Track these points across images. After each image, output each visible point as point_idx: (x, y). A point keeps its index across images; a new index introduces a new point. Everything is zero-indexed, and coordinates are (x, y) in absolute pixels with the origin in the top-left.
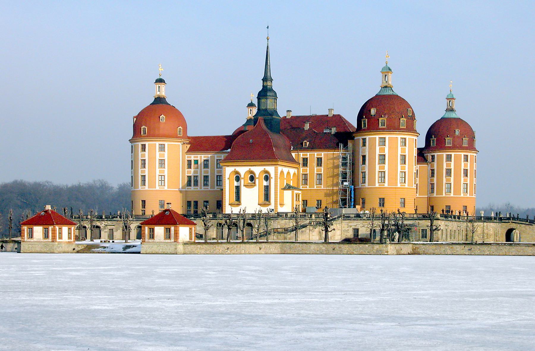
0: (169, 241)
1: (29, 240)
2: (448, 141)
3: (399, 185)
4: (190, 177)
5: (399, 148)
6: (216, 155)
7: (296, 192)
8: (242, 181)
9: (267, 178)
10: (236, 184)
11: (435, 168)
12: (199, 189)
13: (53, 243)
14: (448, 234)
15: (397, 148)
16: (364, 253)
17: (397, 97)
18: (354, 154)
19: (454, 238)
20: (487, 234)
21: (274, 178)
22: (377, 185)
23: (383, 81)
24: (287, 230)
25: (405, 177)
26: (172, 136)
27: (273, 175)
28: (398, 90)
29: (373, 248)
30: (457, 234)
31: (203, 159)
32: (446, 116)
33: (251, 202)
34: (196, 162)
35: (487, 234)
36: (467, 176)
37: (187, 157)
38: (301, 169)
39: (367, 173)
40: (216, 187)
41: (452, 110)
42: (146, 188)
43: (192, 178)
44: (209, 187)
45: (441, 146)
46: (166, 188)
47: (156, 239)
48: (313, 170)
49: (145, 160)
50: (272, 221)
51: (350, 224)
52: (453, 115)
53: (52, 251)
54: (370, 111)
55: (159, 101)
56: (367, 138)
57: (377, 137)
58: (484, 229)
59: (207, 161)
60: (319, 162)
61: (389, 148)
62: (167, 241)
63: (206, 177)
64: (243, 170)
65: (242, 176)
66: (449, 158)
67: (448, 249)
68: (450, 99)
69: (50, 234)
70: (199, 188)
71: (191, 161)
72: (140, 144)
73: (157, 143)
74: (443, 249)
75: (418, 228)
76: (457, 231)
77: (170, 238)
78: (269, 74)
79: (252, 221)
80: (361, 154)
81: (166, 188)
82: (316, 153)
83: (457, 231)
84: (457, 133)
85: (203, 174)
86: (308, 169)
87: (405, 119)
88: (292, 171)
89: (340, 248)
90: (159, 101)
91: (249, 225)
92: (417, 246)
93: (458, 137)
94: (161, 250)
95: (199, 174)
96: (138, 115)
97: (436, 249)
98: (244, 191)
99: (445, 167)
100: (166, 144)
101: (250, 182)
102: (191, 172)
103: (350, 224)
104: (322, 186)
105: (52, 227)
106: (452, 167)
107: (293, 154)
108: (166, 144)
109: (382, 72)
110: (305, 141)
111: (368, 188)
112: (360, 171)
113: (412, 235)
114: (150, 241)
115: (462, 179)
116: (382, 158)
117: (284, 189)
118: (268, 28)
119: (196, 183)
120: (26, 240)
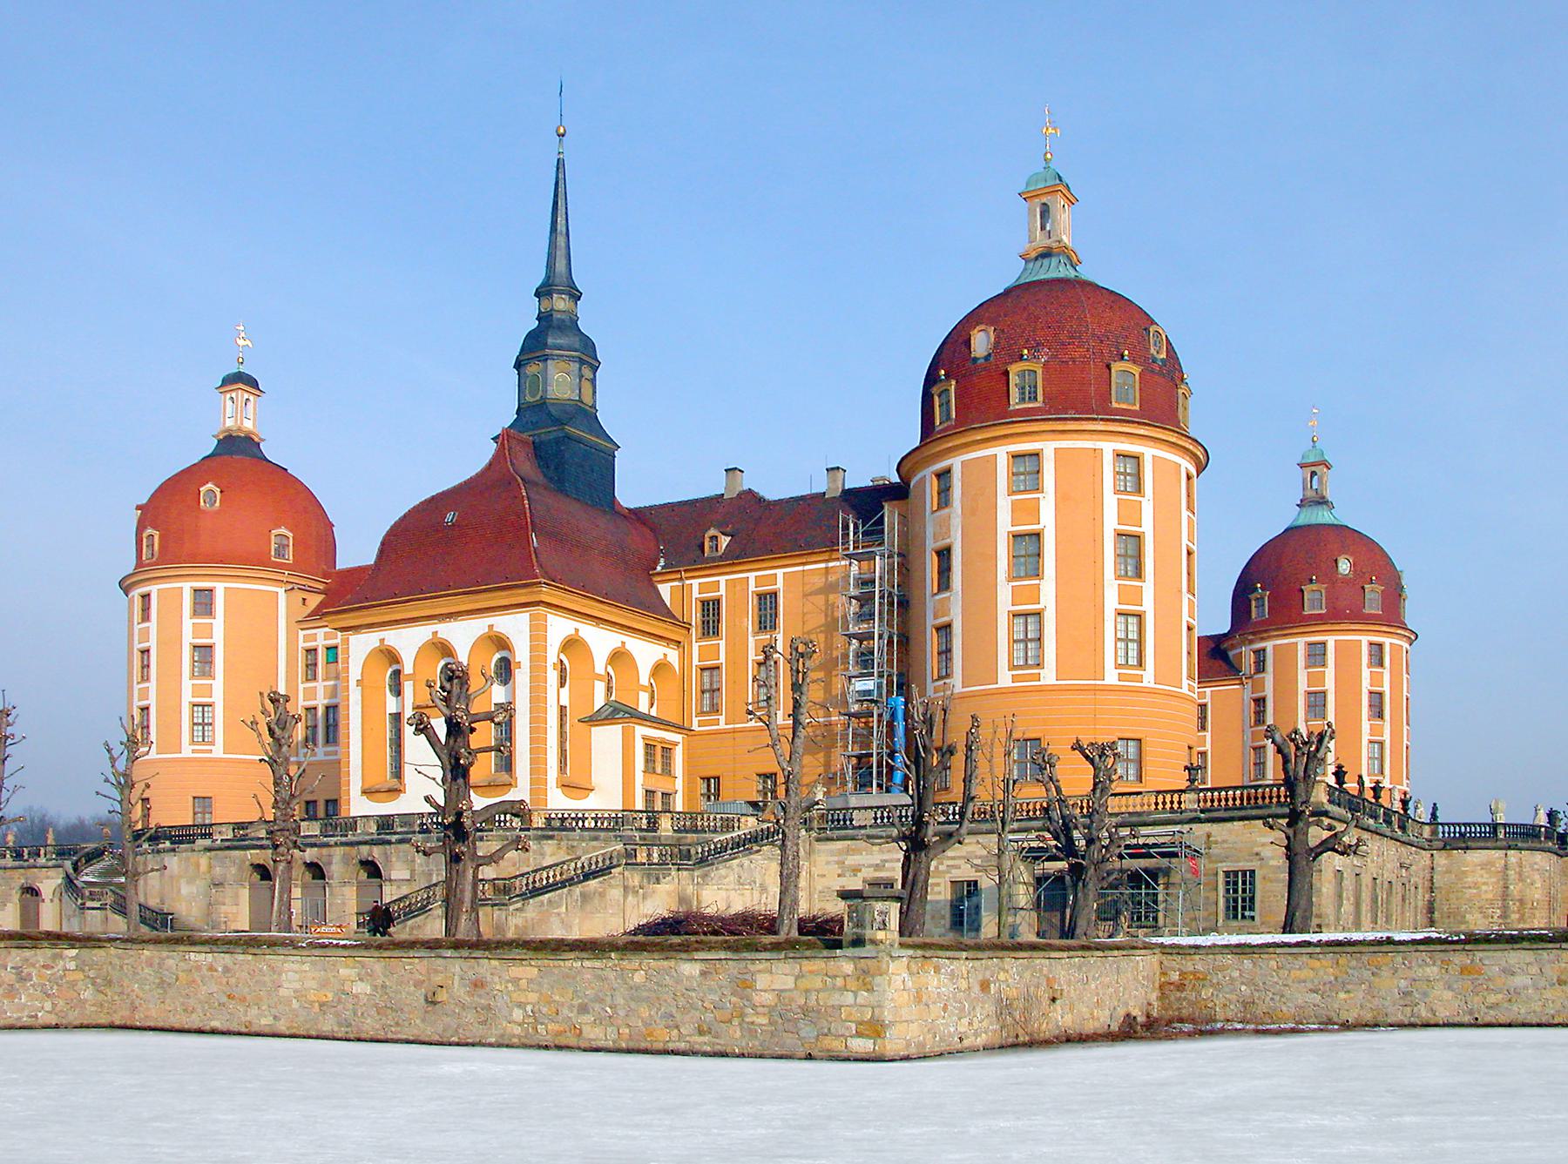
2: (1314, 598)
3: (1111, 677)
5: (1110, 502)
7: (641, 731)
11: (1269, 692)
14: (1366, 896)
16: (663, 1037)
18: (906, 564)
19: (1388, 920)
20: (1521, 901)
21: (526, 664)
22: (1005, 679)
23: (1031, 231)
24: (506, 890)
25: (1140, 642)
26: (256, 560)
27: (522, 654)
29: (744, 986)
30: (1396, 900)
32: (1301, 522)
35: (1521, 901)
36: (1380, 716)
38: (695, 647)
41: (1322, 501)
43: (320, 711)
45: (1288, 615)
46: (218, 751)
48: (741, 644)
51: (851, 860)
52: (1322, 516)
55: (237, 448)
58: (1505, 878)
61: (1061, 499)
65: (408, 669)
66: (1317, 654)
67: (1440, 986)
68: (1314, 467)
73: (187, 587)
74: (1390, 983)
75: (1202, 863)
76: (1397, 887)
78: (560, 266)
79: (377, 853)
80: (931, 545)
81: (218, 751)
82: (752, 575)
83: (1397, 887)
84: (1344, 567)
86: (722, 643)
87: (1136, 370)
88: (646, 653)
89: (478, 984)
90: (237, 448)
92: (1198, 964)
93: (1346, 580)
97: (1340, 984)
99: (1302, 686)
100: (220, 588)
103: (851, 860)
106: (1330, 685)
107: (665, 590)
108: (220, 588)
109: (1027, 197)
110: (712, 532)
111: (963, 697)
112: (931, 622)
113: (1173, 900)
115: (1366, 726)
116: (1028, 544)
117: (595, 719)
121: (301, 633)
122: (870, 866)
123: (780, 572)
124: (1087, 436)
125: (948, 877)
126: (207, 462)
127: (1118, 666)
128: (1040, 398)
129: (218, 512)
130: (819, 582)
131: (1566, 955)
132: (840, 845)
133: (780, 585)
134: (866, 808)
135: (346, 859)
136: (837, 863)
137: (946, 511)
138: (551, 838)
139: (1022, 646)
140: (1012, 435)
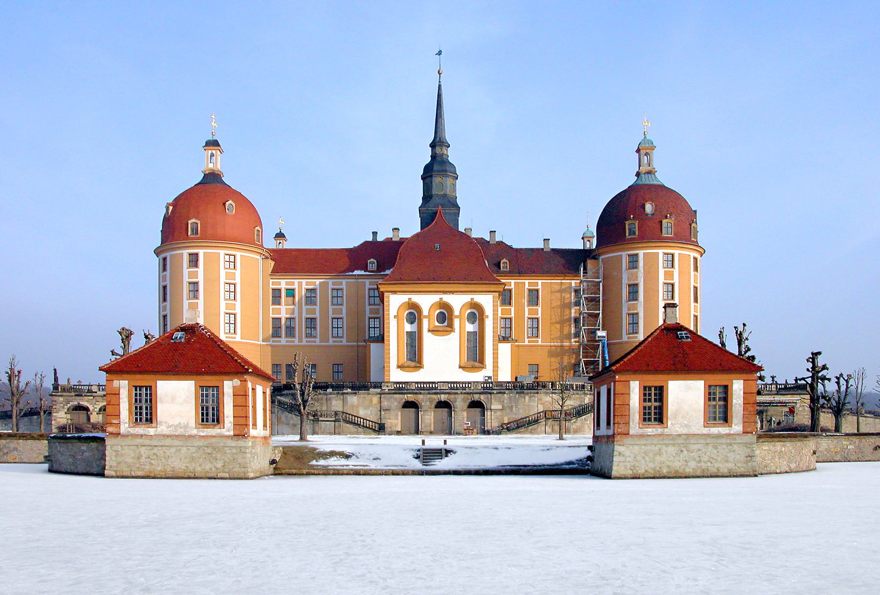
0: (724, 430)
1: (140, 430)
5: (662, 272)
6: (330, 282)
8: (425, 322)
9: (472, 318)
10: (408, 327)
13: (241, 443)
15: (690, 273)
17: (662, 187)
28: (664, 178)
31: (304, 286)
33: (442, 361)
34: (291, 293)
37: (273, 283)
39: (641, 315)
40: (331, 340)
44: (318, 340)
47: (674, 424)
50: (527, 397)
53: (237, 470)
56: (641, 253)
57: (661, 252)
59: (313, 291)
60: (534, 297)
62: (715, 430)
64: (426, 301)
69: (228, 410)
77: (726, 419)
82: (527, 282)
85: (304, 315)
86: (513, 309)
90: (212, 178)
91: (476, 405)
94: (693, 464)
95: (296, 315)
98: (429, 341)
101: (437, 324)
102: (283, 311)
104: (540, 340)
105: (237, 382)
114: (650, 431)
118: (440, 53)
119: (290, 331)
120: (124, 428)
123: (540, 282)
130: (557, 288)
131: (877, 420)
135: (464, 400)
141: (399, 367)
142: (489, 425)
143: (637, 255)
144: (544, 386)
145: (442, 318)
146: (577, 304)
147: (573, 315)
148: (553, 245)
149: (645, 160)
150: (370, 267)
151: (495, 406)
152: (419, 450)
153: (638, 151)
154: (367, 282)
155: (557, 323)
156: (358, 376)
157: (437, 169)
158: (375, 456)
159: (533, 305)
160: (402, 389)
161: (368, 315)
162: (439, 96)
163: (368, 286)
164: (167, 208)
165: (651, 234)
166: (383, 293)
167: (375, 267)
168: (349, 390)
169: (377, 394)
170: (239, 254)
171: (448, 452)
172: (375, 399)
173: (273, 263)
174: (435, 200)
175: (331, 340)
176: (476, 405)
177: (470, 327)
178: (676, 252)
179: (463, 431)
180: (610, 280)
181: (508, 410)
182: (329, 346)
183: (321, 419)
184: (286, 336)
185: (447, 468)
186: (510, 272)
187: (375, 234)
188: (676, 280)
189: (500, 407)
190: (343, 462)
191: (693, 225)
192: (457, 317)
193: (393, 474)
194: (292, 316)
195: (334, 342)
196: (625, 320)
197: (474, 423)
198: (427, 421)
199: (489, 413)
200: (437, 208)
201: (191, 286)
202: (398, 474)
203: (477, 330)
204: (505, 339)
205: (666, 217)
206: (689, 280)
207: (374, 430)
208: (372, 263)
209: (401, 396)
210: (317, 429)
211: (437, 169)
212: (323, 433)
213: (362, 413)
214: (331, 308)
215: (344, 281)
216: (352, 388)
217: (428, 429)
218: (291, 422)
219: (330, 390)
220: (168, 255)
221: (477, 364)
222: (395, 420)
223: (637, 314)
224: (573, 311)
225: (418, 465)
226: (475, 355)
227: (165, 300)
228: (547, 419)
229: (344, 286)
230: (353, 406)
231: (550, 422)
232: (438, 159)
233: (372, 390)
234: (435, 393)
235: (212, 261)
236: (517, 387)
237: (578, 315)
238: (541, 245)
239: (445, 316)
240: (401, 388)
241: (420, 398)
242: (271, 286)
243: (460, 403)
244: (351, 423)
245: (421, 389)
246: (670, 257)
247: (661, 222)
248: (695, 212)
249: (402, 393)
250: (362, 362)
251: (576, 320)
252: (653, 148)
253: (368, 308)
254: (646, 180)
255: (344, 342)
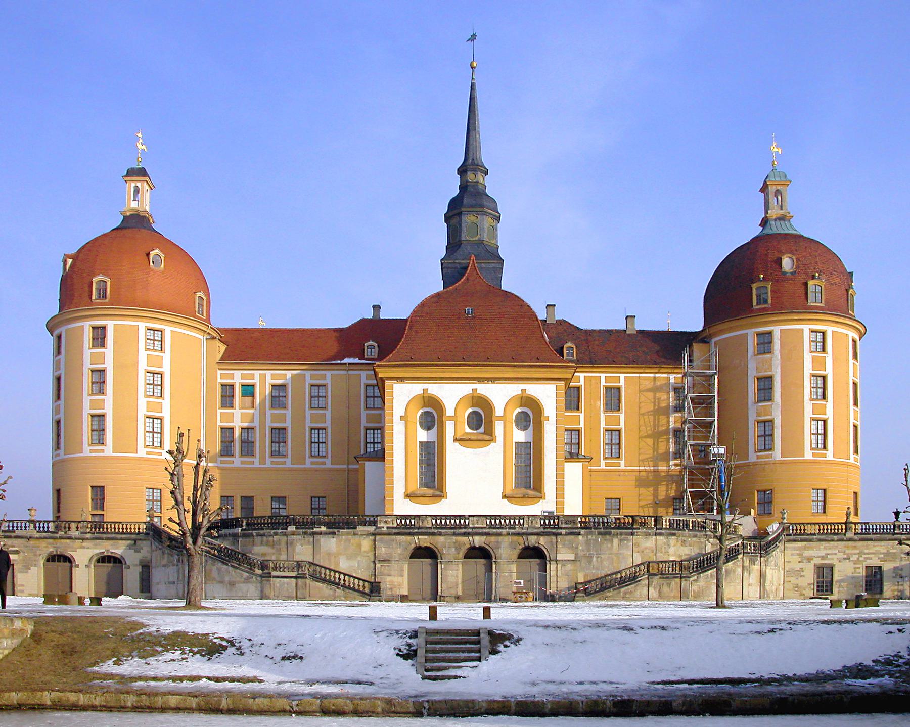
4: (227, 431)
5: (808, 358)
6: (308, 374)
8: (449, 428)
9: (523, 421)
10: (423, 435)
12: (257, 464)
22: (808, 455)
28: (802, 226)
31: (269, 381)
33: (477, 484)
34: (248, 390)
39: (778, 422)
40: (308, 460)
42: (108, 450)
43: (237, 433)
44: (288, 460)
49: (102, 371)
50: (616, 541)
51: (807, 553)
54: (779, 262)
56: (777, 330)
57: (806, 328)
59: (283, 387)
60: (613, 398)
63: (278, 434)
64: (451, 394)
70: (256, 460)
71: (232, 386)
72: (87, 326)
82: (603, 376)
85: (269, 424)
86: (582, 416)
91: (533, 553)
95: (256, 424)
96: (79, 251)
101: (468, 430)
102: (238, 417)
103: (807, 553)
104: (622, 462)
111: (782, 463)
118: (473, 38)
119: (248, 446)
121: (219, 372)
122: (818, 557)
123: (622, 376)
124: (177, 325)
125: (865, 564)
126: (114, 233)
127: (812, 449)
128: (770, 301)
129: (161, 272)
130: (649, 385)
132: (800, 544)
133: (622, 383)
134: (814, 524)
135: (512, 546)
136: (798, 554)
137: (768, 356)
138: (674, 535)
139: (151, 435)
140: (837, 322)
141: (408, 496)
142: (553, 585)
143: (770, 333)
144: (643, 524)
145: (476, 421)
146: (679, 408)
147: (672, 425)
148: (643, 324)
149: (773, 201)
150: (367, 353)
151: (564, 555)
152: (414, 635)
153: (764, 189)
154: (364, 374)
155: (648, 436)
156: (346, 508)
157: (469, 202)
158: (292, 648)
159: (611, 410)
160: (411, 526)
161: (364, 423)
162: (472, 99)
163: (364, 381)
164: (65, 262)
165: (793, 303)
166: (382, 380)
167: (375, 353)
168: (323, 529)
169: (369, 534)
170: (168, 329)
171: (498, 640)
172: (366, 543)
173: (223, 348)
174: (465, 249)
175: (308, 460)
176: (533, 553)
177: (520, 436)
178: (829, 329)
179: (512, 596)
180: (730, 371)
181: (584, 562)
182: (305, 470)
183: (274, 573)
184: (242, 455)
185: (498, 692)
186: (578, 361)
187: (377, 308)
188: (829, 371)
189: (572, 557)
190: (198, 666)
191: (851, 291)
192: (499, 418)
193: (326, 712)
194: (252, 425)
195: (312, 463)
196: (753, 431)
197: (529, 581)
198: (451, 579)
199: (553, 566)
200: (469, 258)
201: (96, 375)
202: (339, 713)
203: (531, 440)
204: (573, 456)
205: (813, 277)
206: (848, 372)
207: (363, 593)
208: (371, 347)
209: (409, 538)
210: (267, 591)
211: (469, 202)
212: (277, 598)
213: (344, 565)
214: (308, 412)
215: (329, 374)
216: (328, 525)
217: (453, 592)
218: (227, 579)
219: (292, 528)
220: (62, 330)
221: (531, 493)
222: (399, 577)
223: (771, 421)
224: (672, 419)
225: (408, 679)
226: (528, 476)
227: (59, 398)
228: (651, 575)
229: (328, 381)
230: (329, 554)
231: (656, 580)
232: (470, 189)
233: (360, 528)
234: (464, 534)
235: (128, 340)
236: (595, 525)
237: (679, 425)
238: (623, 327)
239: (481, 418)
240: (408, 526)
241: (440, 542)
242: (219, 380)
243: (506, 550)
244: (324, 581)
245: (442, 527)
246: (819, 335)
247: (806, 284)
248: (851, 274)
249: (409, 534)
250: (353, 491)
251: (678, 433)
252: (787, 183)
253: (364, 413)
254: (775, 228)
255: (328, 465)
